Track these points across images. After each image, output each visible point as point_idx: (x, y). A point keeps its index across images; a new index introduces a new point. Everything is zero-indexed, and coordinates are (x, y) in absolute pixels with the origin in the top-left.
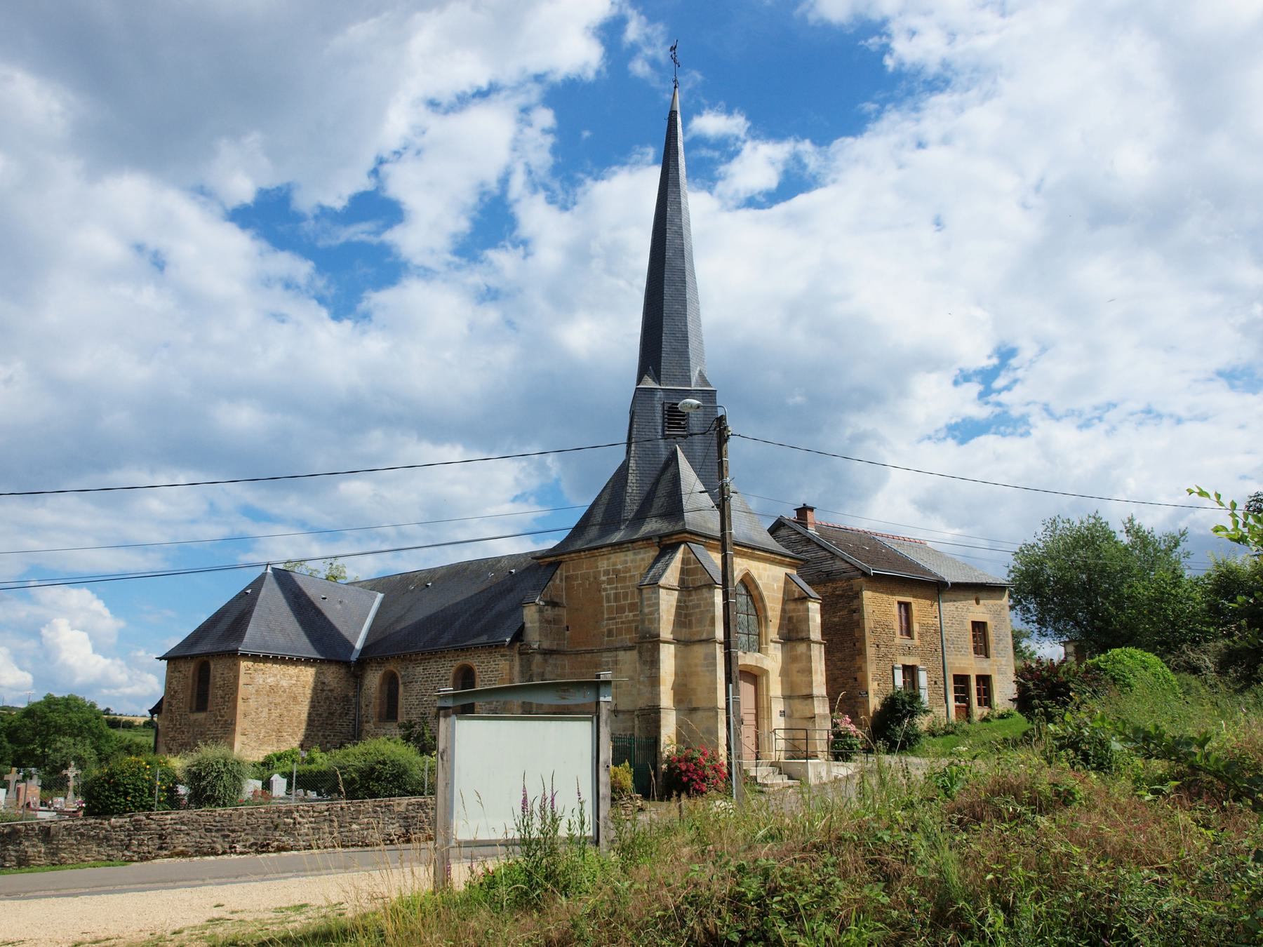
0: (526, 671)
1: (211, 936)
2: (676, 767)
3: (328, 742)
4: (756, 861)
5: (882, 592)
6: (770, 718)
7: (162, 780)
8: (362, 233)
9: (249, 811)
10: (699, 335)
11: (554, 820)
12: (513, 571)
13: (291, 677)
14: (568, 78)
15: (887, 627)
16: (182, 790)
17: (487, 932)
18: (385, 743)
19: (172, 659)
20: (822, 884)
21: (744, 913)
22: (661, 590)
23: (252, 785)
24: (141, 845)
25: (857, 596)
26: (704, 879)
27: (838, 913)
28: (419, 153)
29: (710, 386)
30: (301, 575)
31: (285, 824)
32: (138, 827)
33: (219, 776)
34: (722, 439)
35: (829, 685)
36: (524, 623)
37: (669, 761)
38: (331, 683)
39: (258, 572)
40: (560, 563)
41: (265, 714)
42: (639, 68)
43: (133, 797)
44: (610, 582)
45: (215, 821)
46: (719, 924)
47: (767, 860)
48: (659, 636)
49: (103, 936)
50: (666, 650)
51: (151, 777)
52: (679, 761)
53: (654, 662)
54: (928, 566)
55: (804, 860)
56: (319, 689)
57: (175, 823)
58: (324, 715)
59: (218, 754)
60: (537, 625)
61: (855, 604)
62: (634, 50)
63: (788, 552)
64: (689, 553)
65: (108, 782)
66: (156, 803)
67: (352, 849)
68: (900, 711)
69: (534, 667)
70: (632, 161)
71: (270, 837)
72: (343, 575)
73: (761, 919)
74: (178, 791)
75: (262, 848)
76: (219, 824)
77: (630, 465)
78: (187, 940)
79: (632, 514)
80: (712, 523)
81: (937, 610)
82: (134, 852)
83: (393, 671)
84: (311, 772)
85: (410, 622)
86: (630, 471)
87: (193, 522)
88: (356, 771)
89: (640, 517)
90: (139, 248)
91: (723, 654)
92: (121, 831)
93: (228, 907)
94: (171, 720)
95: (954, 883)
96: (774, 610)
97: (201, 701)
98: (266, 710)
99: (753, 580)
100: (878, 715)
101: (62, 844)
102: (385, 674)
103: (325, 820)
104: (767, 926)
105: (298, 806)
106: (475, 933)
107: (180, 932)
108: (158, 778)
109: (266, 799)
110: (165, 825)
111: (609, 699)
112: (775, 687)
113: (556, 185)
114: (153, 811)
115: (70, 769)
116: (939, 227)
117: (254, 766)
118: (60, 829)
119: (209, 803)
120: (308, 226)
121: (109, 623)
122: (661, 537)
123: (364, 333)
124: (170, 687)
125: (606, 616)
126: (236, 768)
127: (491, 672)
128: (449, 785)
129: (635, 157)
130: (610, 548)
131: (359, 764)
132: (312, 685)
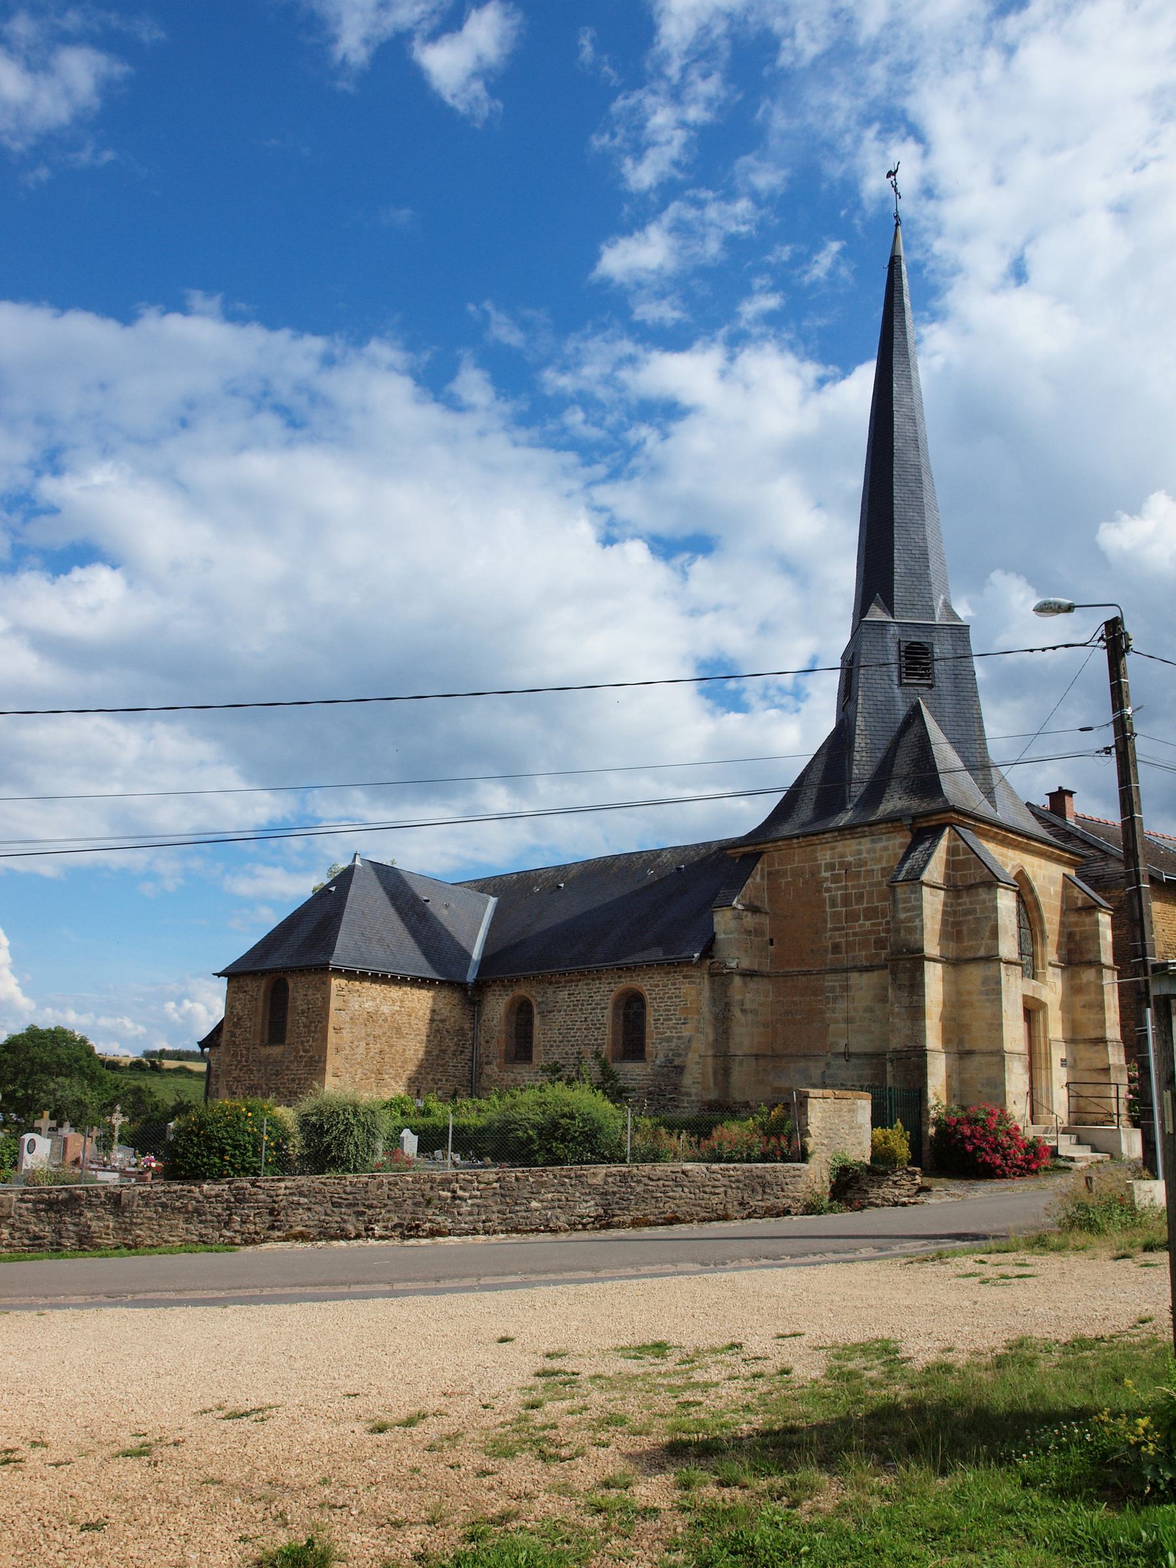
3: (439, 1089)
6: (1049, 1068)
7: (269, 1133)
19: (234, 975)
24: (245, 1223)
31: (440, 1198)
32: (240, 1198)
33: (348, 1130)
37: (937, 1123)
38: (443, 1011)
40: (761, 854)
41: (361, 1050)
43: (233, 1156)
44: (835, 879)
45: (345, 1192)
48: (922, 950)
50: (931, 970)
53: (917, 987)
56: (435, 1018)
64: (955, 840)
65: (197, 1135)
71: (420, 1216)
75: (410, 1230)
76: (350, 1197)
77: (857, 723)
82: (236, 1231)
86: (858, 732)
88: (534, 1126)
92: (217, 1202)
94: (235, 1055)
96: (1051, 923)
97: (276, 1032)
98: (363, 1044)
101: (137, 1218)
103: (495, 1194)
105: (457, 1174)
110: (277, 1196)
114: (259, 1175)
115: (116, 1115)
118: (133, 1197)
122: (914, 818)
124: (232, 1013)
125: (829, 926)
127: (668, 998)
130: (836, 834)
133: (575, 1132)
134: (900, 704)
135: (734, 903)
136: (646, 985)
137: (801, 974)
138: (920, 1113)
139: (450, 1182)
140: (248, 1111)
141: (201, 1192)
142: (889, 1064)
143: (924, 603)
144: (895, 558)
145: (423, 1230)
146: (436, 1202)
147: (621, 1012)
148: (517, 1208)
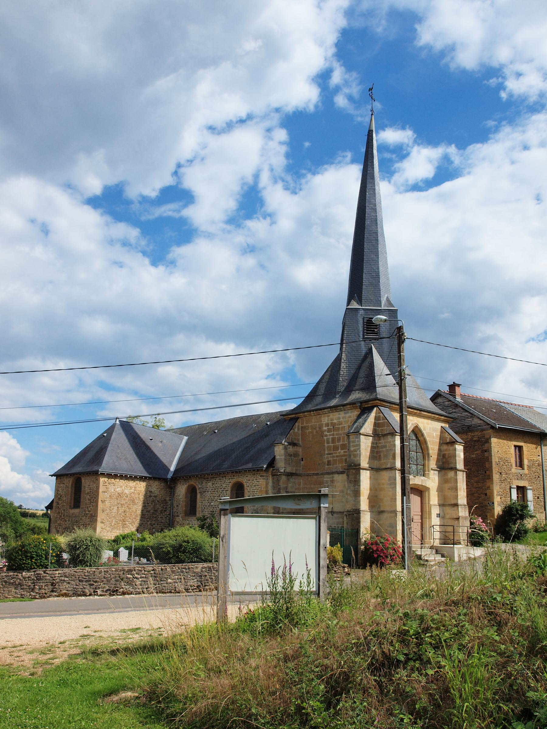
0: (276, 487)
1: (83, 646)
2: (370, 548)
3: (154, 528)
4: (415, 610)
5: (504, 439)
6: (430, 518)
7: (53, 550)
8: (170, 211)
9: (105, 570)
10: (387, 275)
11: (291, 581)
12: (268, 423)
13: (131, 488)
14: (297, 110)
15: (507, 461)
16: (65, 556)
17: (248, 649)
18: (188, 530)
19: (59, 475)
20: (457, 627)
21: (408, 643)
22: (361, 436)
23: (107, 554)
24: (41, 589)
25: (488, 441)
26: (383, 621)
27: (467, 645)
28: (203, 159)
29: (393, 307)
30: (136, 424)
31: (127, 578)
32: (39, 578)
33: (87, 548)
34: (401, 341)
35: (469, 498)
36: (275, 456)
38: (156, 492)
39: (110, 423)
40: (298, 418)
41: (115, 510)
42: (341, 101)
43: (36, 560)
44: (329, 431)
45: (85, 575)
46: (391, 649)
47: (423, 610)
48: (360, 465)
49: (18, 643)
50: (364, 474)
51: (46, 548)
52: (372, 544)
53: (356, 482)
54: (534, 423)
55: (446, 611)
56: (148, 496)
57: (61, 576)
58: (151, 512)
59: (86, 535)
60: (283, 457)
61: (486, 446)
62: (337, 89)
63: (443, 413)
64: (379, 413)
65: (21, 551)
66: (49, 564)
67: (168, 594)
68: (514, 515)
69: (281, 484)
70: (337, 161)
72: (163, 424)
73: (418, 647)
74: (62, 557)
75: (113, 592)
76: (87, 577)
77: (342, 357)
78: (68, 647)
79: (343, 388)
80: (394, 394)
81: (540, 451)
82: (37, 593)
83: (193, 485)
84: (143, 546)
85: (204, 455)
86: (342, 361)
87: (69, 391)
88: (171, 546)
89: (349, 390)
90: (33, 221)
91: (400, 477)
93: (93, 628)
95: (541, 629)
96: (433, 450)
97: (76, 503)
98: (116, 508)
99: (420, 431)
100: (500, 517)
102: (189, 486)
104: (422, 651)
106: (241, 649)
107: (63, 643)
108: (51, 549)
109: (116, 562)
110: (55, 577)
111: (327, 505)
112: (434, 499)
113: (289, 178)
114: (48, 568)
116: (539, 202)
117: (109, 542)
119: (81, 564)
120: (135, 207)
121: (20, 453)
122: (361, 403)
123: (171, 273)
124: (57, 493)
125: (326, 452)
126: (97, 543)
128: (227, 557)
129: (339, 159)
131: (173, 542)
132: (144, 493)
133: (189, 548)
134: (363, 347)
135: (283, 442)
136: (245, 480)
137: (314, 474)
138: (357, 539)
139: (132, 571)
140: (44, 540)
141: (22, 576)
142: (345, 517)
143: (377, 299)
144: (364, 278)
145: (119, 592)
146: (125, 579)
147: (235, 492)
148: (162, 582)
